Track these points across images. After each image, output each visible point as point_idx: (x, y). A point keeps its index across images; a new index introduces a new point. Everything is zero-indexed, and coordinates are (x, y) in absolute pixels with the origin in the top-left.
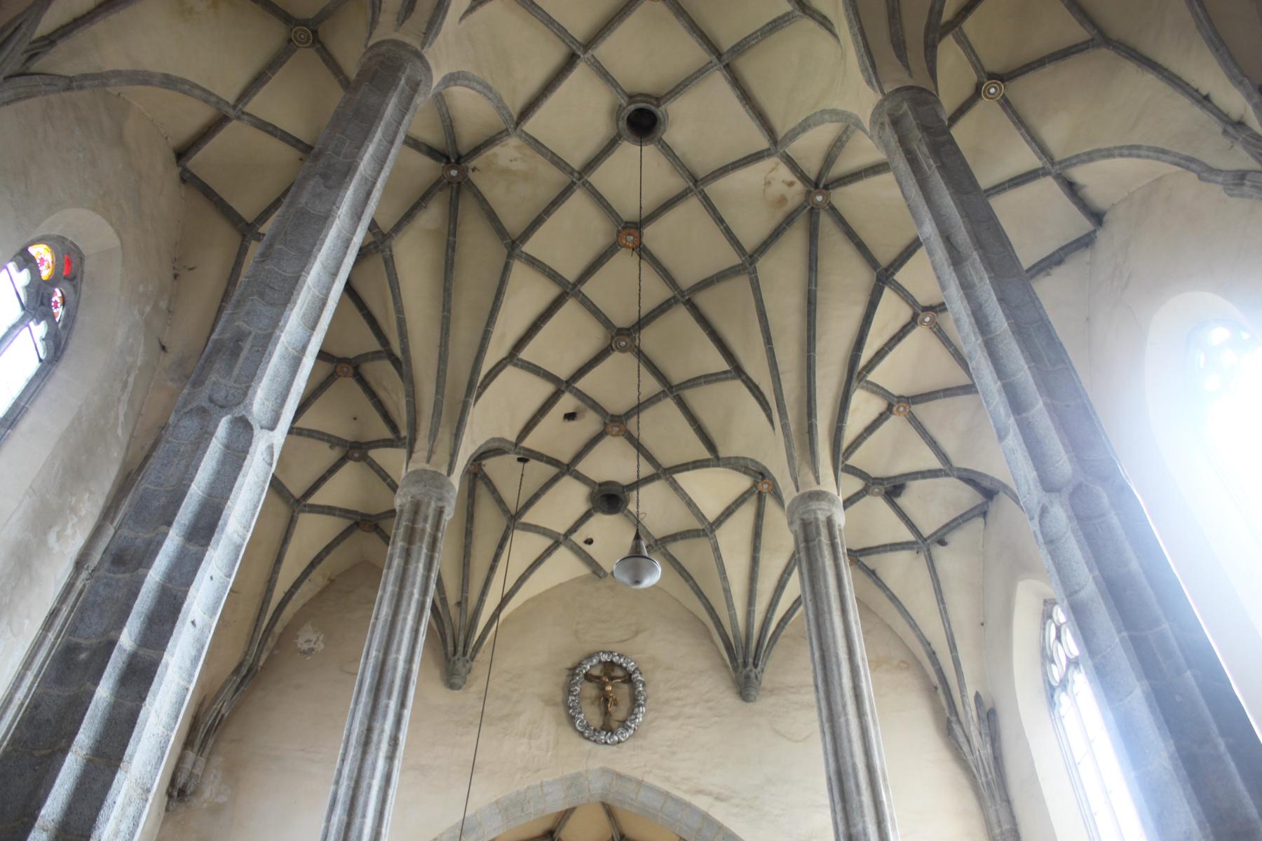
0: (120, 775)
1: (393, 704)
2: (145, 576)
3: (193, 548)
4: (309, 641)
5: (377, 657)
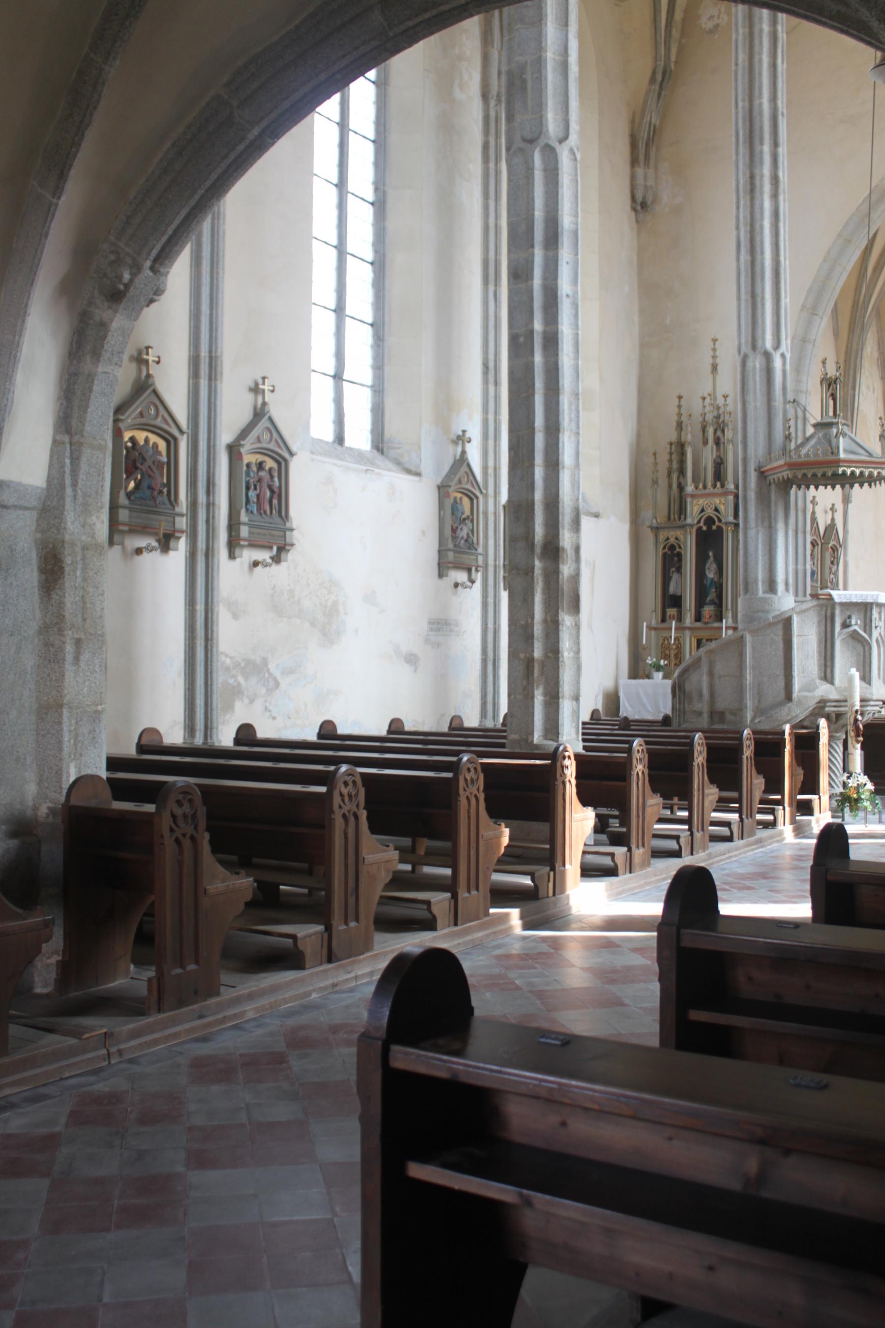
0: (561, 397)
1: (766, 148)
2: (532, 285)
3: (551, 253)
4: (712, 17)
5: (743, 108)
